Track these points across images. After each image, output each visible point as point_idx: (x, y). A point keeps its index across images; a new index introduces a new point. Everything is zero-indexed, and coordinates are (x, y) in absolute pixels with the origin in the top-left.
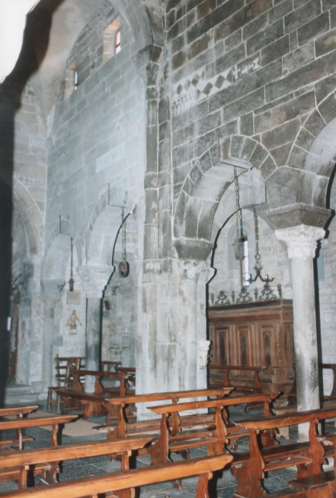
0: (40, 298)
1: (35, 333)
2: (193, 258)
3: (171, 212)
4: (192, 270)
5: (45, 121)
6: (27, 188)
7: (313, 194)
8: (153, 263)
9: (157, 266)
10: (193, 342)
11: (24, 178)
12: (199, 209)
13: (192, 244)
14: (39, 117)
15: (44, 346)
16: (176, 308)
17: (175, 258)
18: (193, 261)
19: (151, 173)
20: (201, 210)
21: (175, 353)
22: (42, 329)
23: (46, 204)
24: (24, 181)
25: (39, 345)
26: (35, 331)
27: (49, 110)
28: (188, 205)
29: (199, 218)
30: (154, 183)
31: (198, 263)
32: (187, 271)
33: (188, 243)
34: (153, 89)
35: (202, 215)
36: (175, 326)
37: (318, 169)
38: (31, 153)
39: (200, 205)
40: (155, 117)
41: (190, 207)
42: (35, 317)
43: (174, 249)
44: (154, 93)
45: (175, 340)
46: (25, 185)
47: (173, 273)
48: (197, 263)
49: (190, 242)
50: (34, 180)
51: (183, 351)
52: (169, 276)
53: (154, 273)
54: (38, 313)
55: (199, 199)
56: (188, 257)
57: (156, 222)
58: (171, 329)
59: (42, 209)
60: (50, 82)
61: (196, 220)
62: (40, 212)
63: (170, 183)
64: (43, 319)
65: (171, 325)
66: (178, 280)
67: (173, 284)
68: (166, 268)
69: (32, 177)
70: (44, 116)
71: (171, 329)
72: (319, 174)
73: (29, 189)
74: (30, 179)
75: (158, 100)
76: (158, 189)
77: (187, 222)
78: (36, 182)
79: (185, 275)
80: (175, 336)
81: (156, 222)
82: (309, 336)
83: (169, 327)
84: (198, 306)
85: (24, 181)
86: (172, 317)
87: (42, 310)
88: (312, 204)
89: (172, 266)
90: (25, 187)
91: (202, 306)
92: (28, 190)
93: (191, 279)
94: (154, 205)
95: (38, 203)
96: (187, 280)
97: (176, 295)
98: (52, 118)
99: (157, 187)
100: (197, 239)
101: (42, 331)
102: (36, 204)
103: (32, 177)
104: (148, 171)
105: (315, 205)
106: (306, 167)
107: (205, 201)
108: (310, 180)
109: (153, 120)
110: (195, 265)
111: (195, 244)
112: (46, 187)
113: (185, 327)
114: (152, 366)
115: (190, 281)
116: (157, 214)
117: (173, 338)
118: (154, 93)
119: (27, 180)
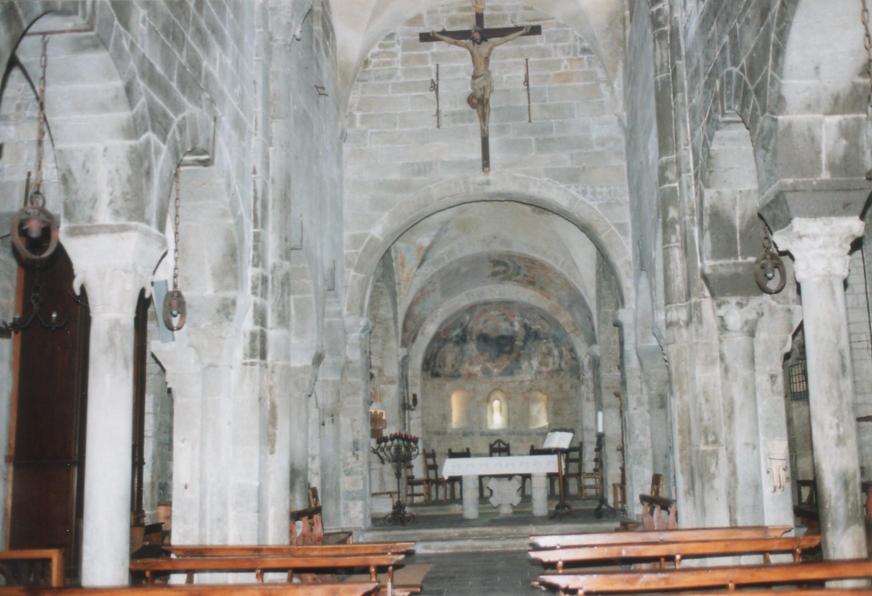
0: (640, 378)
1: (637, 436)
2: (734, 293)
3: (692, 221)
4: (735, 316)
5: (612, 92)
6: (595, 204)
7: (824, 156)
8: (677, 310)
9: (683, 315)
10: (747, 444)
11: (589, 189)
12: (734, 208)
13: (723, 271)
14: (603, 86)
15: (654, 457)
16: (230, 423)
17: (705, 297)
18: (733, 300)
19: (664, 158)
20: (737, 208)
21: (717, 464)
22: (648, 428)
23: (630, 225)
24: (589, 195)
25: (646, 454)
26: (637, 432)
27: (615, 70)
28: (707, 204)
29: (737, 223)
30: (670, 175)
31: (748, 301)
32: (726, 318)
33: (714, 270)
34: (659, 12)
35: (743, 217)
36: (714, 416)
37: (826, 105)
38: (598, 149)
39: (734, 200)
40: (665, 59)
41: (712, 207)
42: (635, 409)
43: (701, 282)
44: (661, 18)
45: (716, 442)
46: (592, 200)
47: (705, 323)
48: (744, 302)
49: (719, 268)
50: (605, 190)
51: (731, 460)
52: (697, 330)
53: (680, 327)
54: (640, 402)
55: (726, 191)
56: (723, 294)
57: (677, 241)
58: (705, 423)
59: (625, 234)
60: (607, 26)
61: (732, 227)
62: (622, 238)
63: (689, 171)
64: (649, 412)
65: (706, 415)
66: (715, 335)
67: (706, 344)
68: (694, 317)
69: (601, 187)
70: (610, 84)
71: (705, 423)
72: (832, 113)
73: (599, 205)
74: (598, 189)
75: (667, 28)
76: (676, 184)
77: (712, 234)
78: (609, 193)
79: (723, 327)
80: (714, 434)
81: (677, 241)
82: (831, 427)
83: (701, 420)
84: (762, 380)
85: (589, 195)
86: (707, 401)
87: (645, 398)
88: (825, 175)
89: (700, 311)
90: (591, 203)
91: (773, 377)
92: (596, 208)
93: (736, 332)
94: (673, 213)
95: (616, 225)
96: (728, 335)
97: (712, 362)
98: (621, 82)
99: (674, 182)
100: (740, 260)
101: (648, 432)
102: (613, 228)
103: (601, 187)
104: (660, 157)
105: (833, 175)
106: (788, 109)
107: (740, 192)
108: (809, 129)
109: (662, 65)
110: (740, 305)
111: (733, 270)
112: (627, 198)
113: (730, 416)
114: (687, 487)
115: (733, 334)
116: (678, 227)
117: (711, 438)
118: (661, 18)
119: (594, 193)
